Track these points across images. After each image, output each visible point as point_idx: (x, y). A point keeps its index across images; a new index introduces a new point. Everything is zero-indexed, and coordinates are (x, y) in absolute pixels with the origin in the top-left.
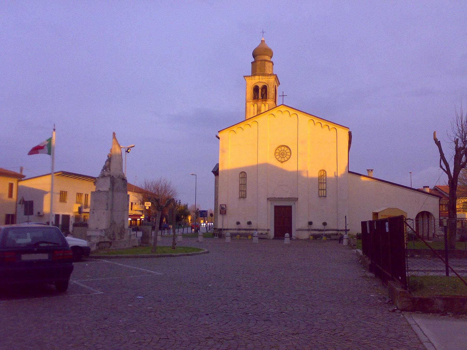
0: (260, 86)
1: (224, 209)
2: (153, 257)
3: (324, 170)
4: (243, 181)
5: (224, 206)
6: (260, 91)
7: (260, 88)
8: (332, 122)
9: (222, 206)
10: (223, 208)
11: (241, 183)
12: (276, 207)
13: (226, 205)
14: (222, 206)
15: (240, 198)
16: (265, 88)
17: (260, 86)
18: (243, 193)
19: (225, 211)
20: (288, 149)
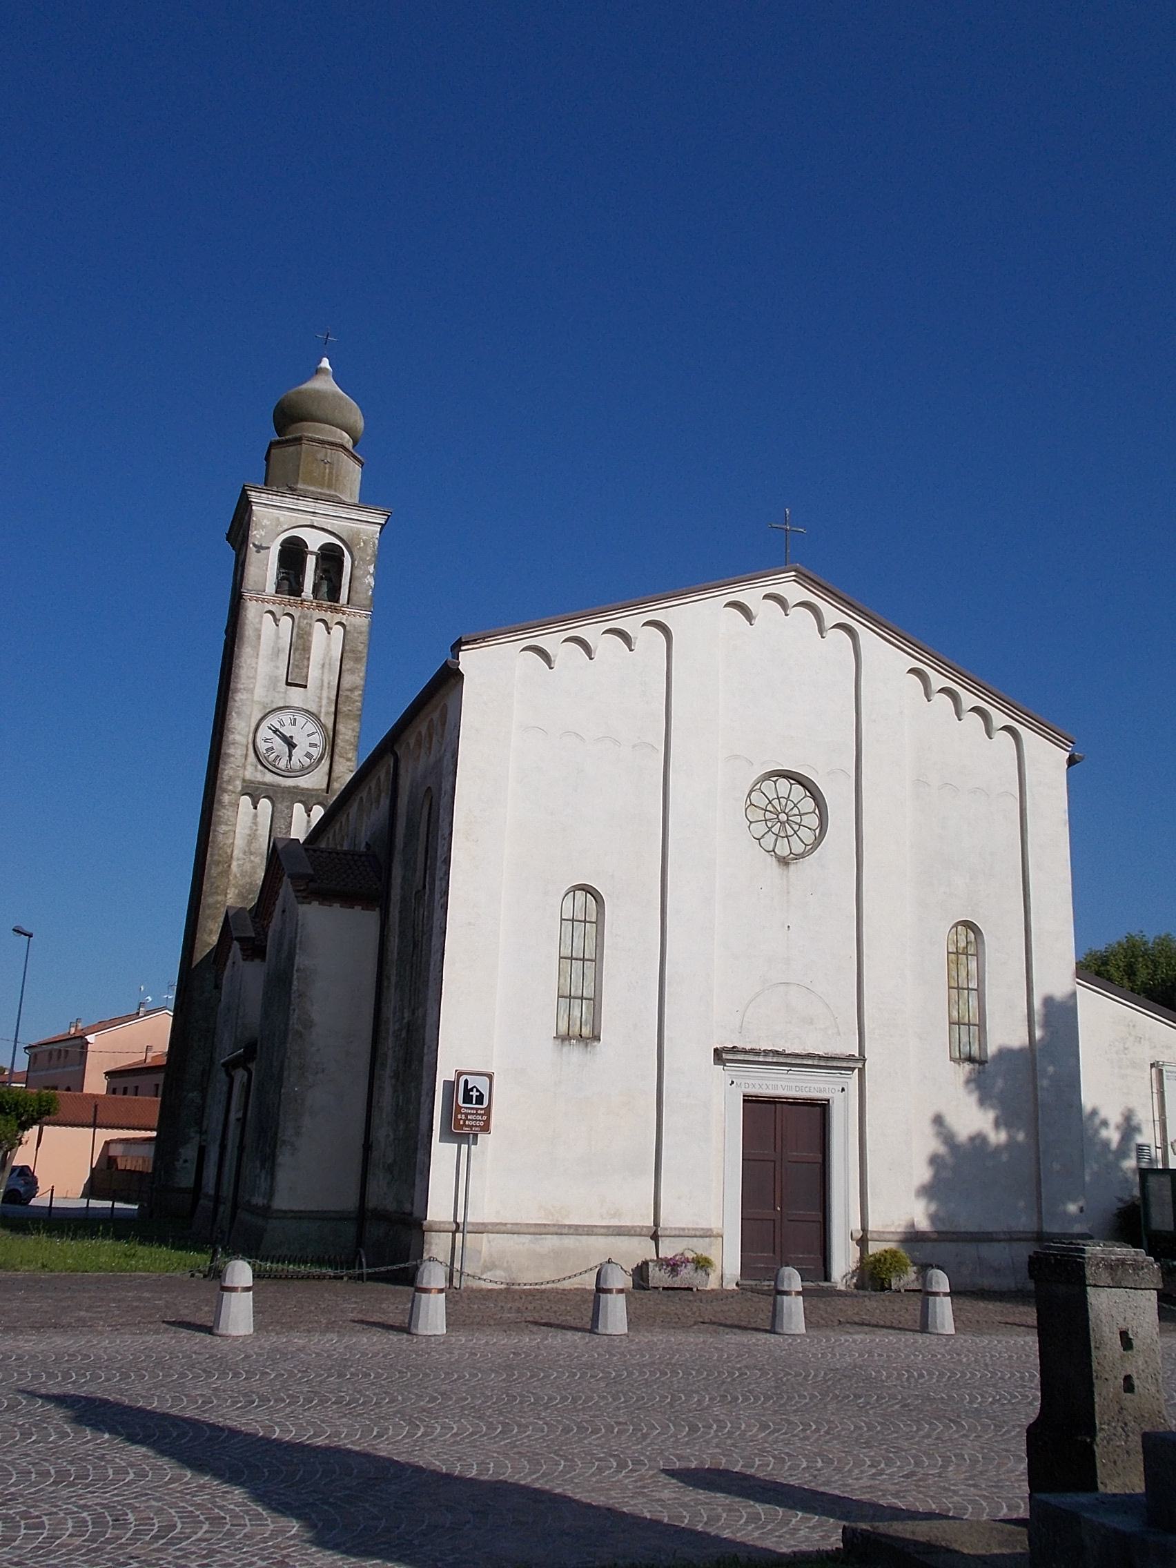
0: (315, 541)
1: (480, 1099)
2: (904, 1520)
3: (968, 925)
4: (578, 942)
5: (481, 1084)
6: (311, 561)
7: (312, 553)
8: (18, 1008)
9: (466, 1082)
10: (474, 1093)
11: (567, 953)
12: (748, 1100)
13: (490, 1076)
14: (466, 1082)
15: (564, 1038)
16: (331, 558)
17: (315, 541)
18: (576, 1013)
19: (488, 1111)
20: (775, 782)
